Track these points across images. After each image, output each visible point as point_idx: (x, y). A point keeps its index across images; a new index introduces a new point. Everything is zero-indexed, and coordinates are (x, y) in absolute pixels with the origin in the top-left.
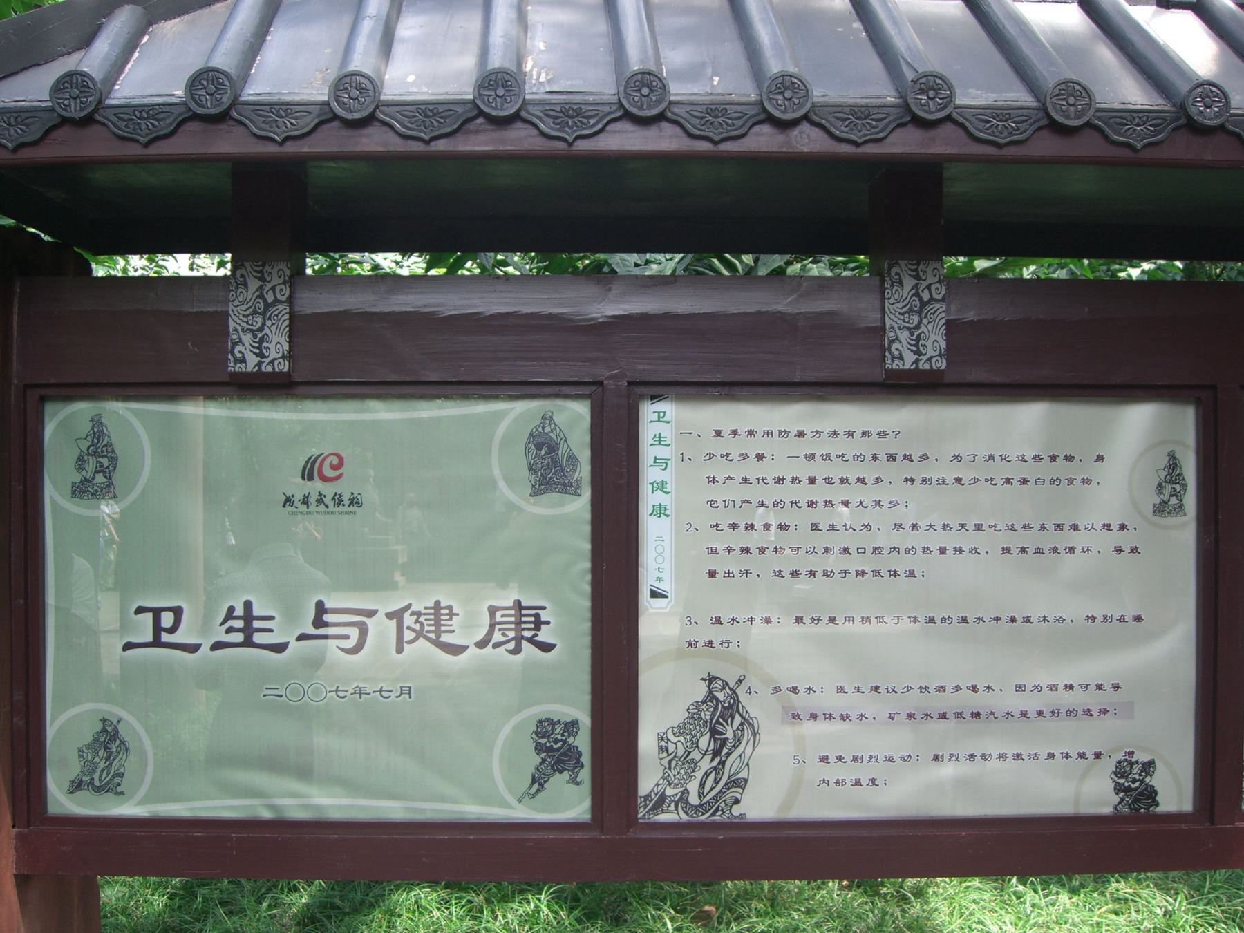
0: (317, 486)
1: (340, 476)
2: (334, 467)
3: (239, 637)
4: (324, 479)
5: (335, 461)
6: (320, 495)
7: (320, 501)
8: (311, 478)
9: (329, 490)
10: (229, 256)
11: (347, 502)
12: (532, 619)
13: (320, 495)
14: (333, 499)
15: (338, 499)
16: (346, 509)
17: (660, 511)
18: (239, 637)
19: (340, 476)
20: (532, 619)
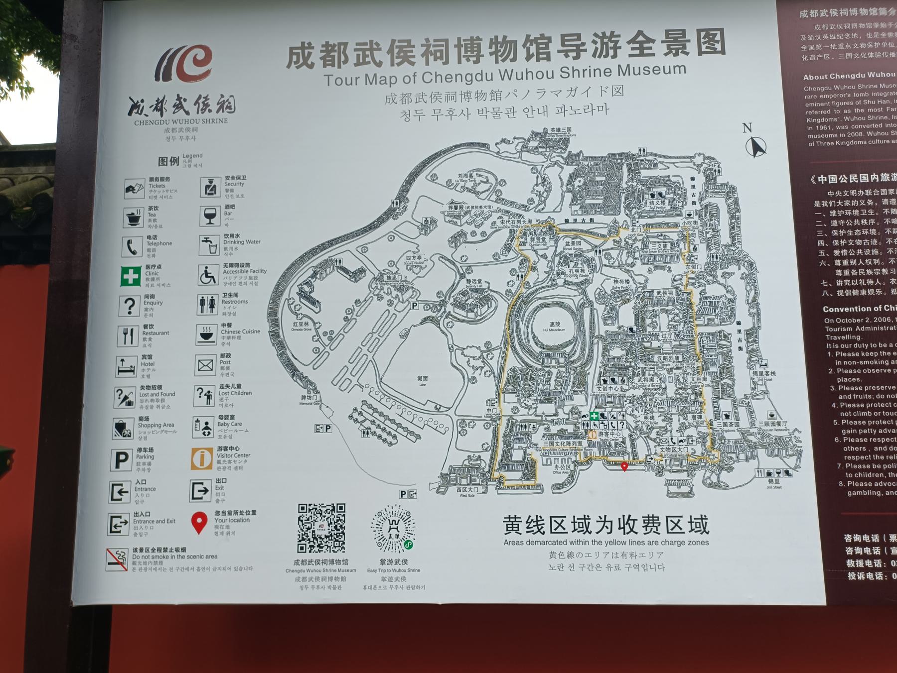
0: (174, 87)
1: (207, 73)
2: (197, 63)
3: (638, 52)
4: (184, 77)
5: (201, 55)
6: (179, 98)
7: (179, 106)
8: (167, 77)
9: (190, 91)
10: (848, 538)
11: (214, 106)
12: (567, 43)
13: (179, 98)
14: (197, 103)
15: (203, 104)
16: (213, 115)
17: (324, 527)
18: (638, 52)
19: (207, 73)
20: (567, 43)
